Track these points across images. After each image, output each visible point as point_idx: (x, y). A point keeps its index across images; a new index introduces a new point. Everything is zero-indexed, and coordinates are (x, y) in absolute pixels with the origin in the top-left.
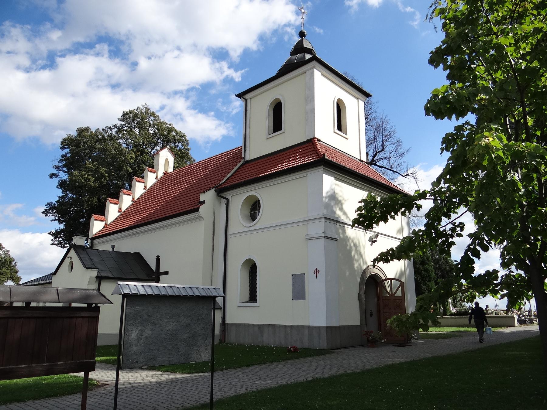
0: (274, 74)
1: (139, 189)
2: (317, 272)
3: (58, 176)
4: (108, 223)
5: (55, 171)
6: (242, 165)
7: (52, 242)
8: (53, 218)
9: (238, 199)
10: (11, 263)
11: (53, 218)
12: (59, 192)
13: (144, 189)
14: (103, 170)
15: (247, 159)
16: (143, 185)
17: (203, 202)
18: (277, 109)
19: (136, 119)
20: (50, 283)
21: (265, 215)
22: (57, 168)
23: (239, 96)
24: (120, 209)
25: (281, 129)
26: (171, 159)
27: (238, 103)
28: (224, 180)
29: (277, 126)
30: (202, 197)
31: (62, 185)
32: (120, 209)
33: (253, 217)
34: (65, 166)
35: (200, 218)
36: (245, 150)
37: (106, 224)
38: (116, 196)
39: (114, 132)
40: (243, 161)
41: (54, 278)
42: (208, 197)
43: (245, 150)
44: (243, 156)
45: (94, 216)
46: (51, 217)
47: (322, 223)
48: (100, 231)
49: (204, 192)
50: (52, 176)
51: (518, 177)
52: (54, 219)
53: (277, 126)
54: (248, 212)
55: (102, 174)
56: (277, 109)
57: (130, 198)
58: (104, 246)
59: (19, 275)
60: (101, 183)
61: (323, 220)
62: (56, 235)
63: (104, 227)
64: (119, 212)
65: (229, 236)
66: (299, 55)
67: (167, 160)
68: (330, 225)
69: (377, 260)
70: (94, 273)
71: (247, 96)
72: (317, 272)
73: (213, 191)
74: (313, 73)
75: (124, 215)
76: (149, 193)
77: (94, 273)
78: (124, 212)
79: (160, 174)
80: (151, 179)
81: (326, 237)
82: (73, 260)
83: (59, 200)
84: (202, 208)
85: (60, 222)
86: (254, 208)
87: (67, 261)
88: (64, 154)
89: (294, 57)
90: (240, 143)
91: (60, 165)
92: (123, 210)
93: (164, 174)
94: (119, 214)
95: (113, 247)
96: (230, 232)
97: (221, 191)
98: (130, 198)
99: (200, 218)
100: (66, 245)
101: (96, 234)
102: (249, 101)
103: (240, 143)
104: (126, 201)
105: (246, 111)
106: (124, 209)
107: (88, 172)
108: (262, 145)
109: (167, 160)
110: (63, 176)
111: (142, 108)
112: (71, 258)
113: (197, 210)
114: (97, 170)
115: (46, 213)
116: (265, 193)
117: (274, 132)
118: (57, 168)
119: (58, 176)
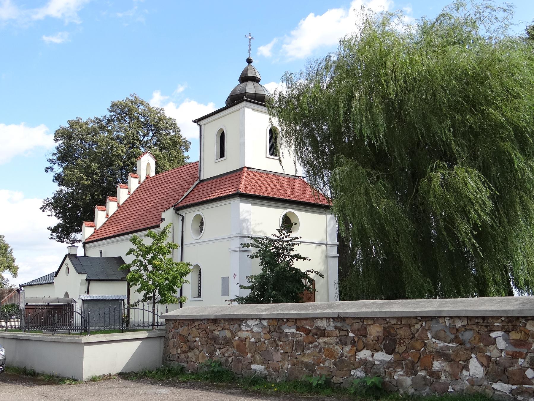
1: (123, 194)
3: (53, 169)
4: (97, 229)
5: (50, 165)
6: (197, 184)
7: (51, 237)
8: (50, 213)
9: (190, 215)
10: (6, 250)
11: (50, 213)
12: (56, 187)
13: (128, 194)
14: (94, 166)
15: (202, 178)
16: (127, 190)
19: (124, 111)
20: (53, 283)
22: (51, 161)
24: (107, 215)
26: (153, 162)
28: (182, 199)
30: (163, 215)
31: (58, 179)
32: (107, 215)
34: (58, 159)
37: (95, 229)
38: (103, 203)
39: (104, 123)
40: (198, 180)
41: (56, 280)
42: (168, 215)
45: (85, 224)
46: (48, 212)
48: (91, 236)
49: (164, 211)
50: (47, 170)
52: (50, 214)
55: (94, 170)
57: (116, 204)
58: (94, 252)
59: (16, 263)
60: (93, 179)
62: (55, 230)
63: (94, 232)
64: (106, 217)
67: (148, 164)
70: (84, 277)
71: (202, 123)
74: (244, 111)
75: (111, 220)
76: (132, 196)
77: (84, 277)
78: (111, 217)
79: (143, 178)
80: (134, 184)
82: (69, 266)
83: (54, 197)
85: (58, 217)
87: (64, 266)
88: (58, 145)
91: (55, 158)
92: (110, 216)
93: (147, 178)
94: (107, 219)
95: (101, 251)
97: (178, 209)
98: (116, 204)
100: (64, 240)
101: (87, 239)
102: (203, 127)
104: (112, 207)
105: (201, 136)
106: (110, 214)
107: (80, 170)
109: (148, 164)
110: (58, 169)
111: (130, 98)
112: (67, 264)
114: (88, 167)
115: (43, 209)
116: (207, 212)
118: (51, 161)
119: (53, 169)
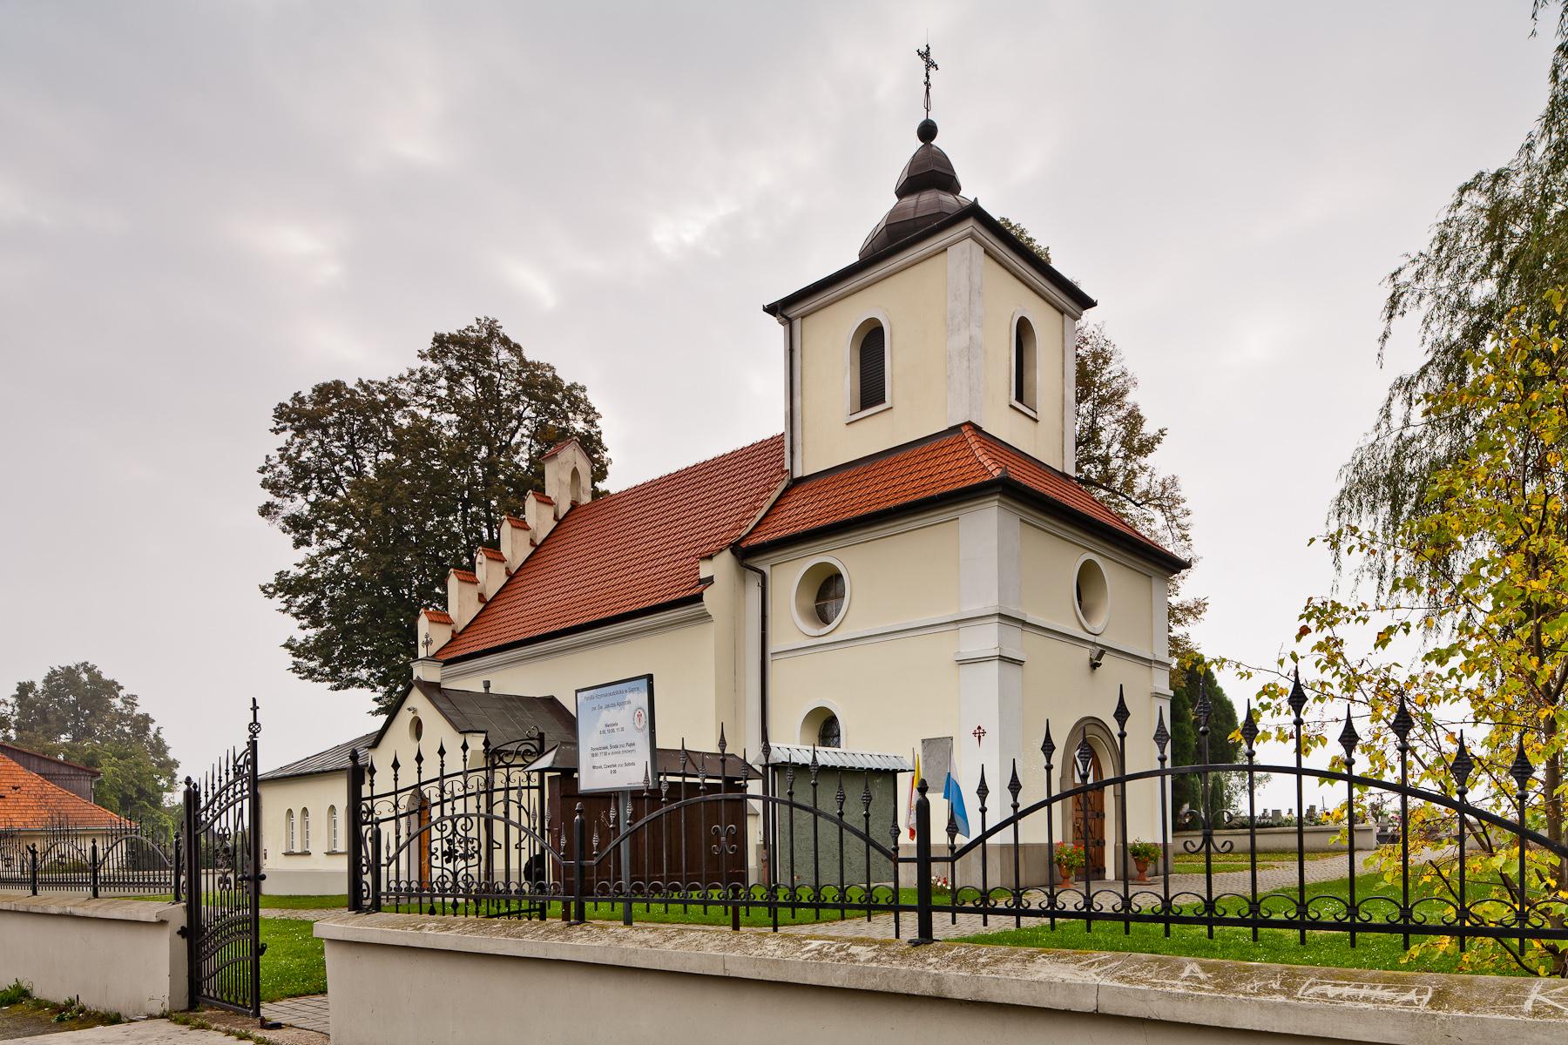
0: (854, 258)
2: (979, 733)
9: (788, 576)
15: (798, 474)
17: (710, 580)
18: (871, 341)
21: (855, 614)
23: (772, 309)
25: (883, 401)
27: (774, 329)
29: (871, 391)
33: (822, 617)
35: (705, 617)
36: (792, 452)
43: (792, 452)
44: (787, 466)
47: (993, 627)
51: (1397, 557)
53: (871, 391)
54: (810, 603)
56: (871, 341)
61: (997, 619)
65: (769, 658)
66: (927, 197)
68: (1015, 632)
69: (414, 711)
71: (794, 312)
72: (979, 733)
73: (727, 554)
81: (1002, 658)
84: (708, 594)
86: (825, 592)
89: (910, 201)
90: (778, 426)
96: (771, 649)
97: (747, 555)
99: (705, 617)
102: (797, 323)
103: (778, 426)
105: (791, 350)
108: (836, 438)
113: (698, 598)
117: (863, 407)
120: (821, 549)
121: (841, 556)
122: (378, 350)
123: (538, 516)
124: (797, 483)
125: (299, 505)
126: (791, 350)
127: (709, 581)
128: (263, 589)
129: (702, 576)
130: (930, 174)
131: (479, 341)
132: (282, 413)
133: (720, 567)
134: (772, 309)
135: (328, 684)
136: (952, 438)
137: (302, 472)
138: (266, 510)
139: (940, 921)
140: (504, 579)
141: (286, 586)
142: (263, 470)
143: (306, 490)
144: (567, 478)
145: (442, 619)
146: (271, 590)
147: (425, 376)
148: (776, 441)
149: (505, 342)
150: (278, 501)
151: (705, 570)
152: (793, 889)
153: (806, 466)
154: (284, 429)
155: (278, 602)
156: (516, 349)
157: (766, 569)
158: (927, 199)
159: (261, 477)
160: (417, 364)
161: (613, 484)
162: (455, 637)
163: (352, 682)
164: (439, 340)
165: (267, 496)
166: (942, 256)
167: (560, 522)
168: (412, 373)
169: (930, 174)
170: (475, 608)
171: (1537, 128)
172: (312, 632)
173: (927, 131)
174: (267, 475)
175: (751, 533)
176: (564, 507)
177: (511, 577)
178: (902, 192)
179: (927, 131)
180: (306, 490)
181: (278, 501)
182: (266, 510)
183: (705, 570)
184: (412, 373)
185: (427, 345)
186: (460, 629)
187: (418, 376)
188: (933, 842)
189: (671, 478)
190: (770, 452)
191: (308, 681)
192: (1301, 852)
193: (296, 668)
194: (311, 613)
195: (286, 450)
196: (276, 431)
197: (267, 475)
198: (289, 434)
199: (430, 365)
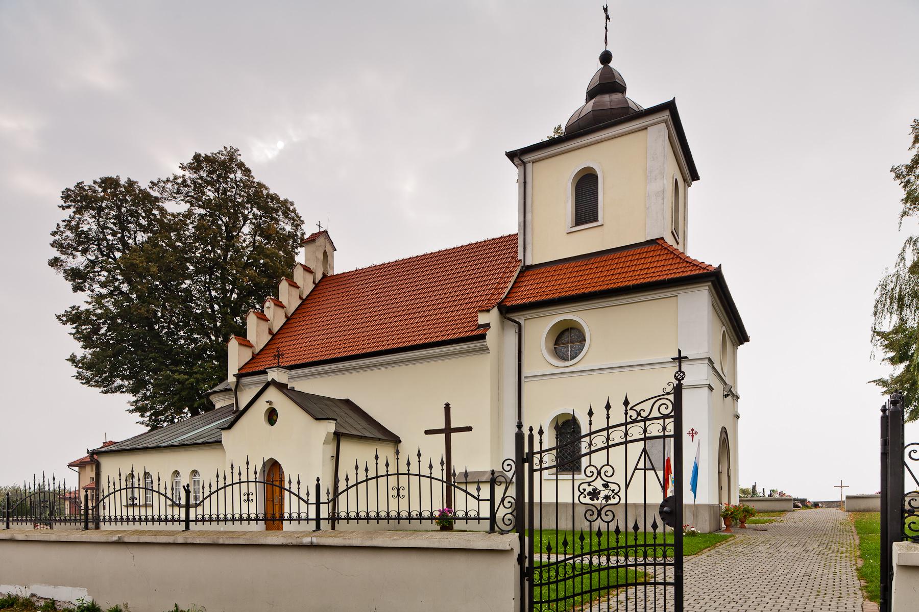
9: (539, 328)
15: (528, 263)
23: (511, 155)
25: (596, 220)
27: (512, 171)
35: (485, 349)
36: (525, 248)
43: (525, 248)
44: (520, 256)
54: (552, 346)
65: (523, 379)
71: (526, 158)
86: (567, 341)
97: (507, 311)
99: (485, 349)
102: (529, 166)
105: (525, 183)
108: (556, 239)
113: (483, 337)
117: (578, 223)
120: (572, 309)
121: (586, 317)
122: (157, 161)
123: (304, 279)
124: (527, 269)
125: (79, 261)
126: (525, 183)
127: (487, 326)
128: (59, 317)
129: (480, 322)
130: (608, 84)
131: (223, 162)
132: (66, 195)
133: (491, 318)
134: (511, 155)
135: (102, 389)
136: (653, 247)
137: (83, 241)
138: (55, 263)
139: (192, 524)
140: (284, 320)
141: (75, 317)
142: (54, 234)
143: (84, 252)
144: (321, 256)
145: (245, 343)
146: (64, 319)
147: (185, 181)
148: (513, 238)
149: (241, 165)
150: (63, 257)
151: (483, 319)
152: (290, 514)
153: (533, 259)
154: (69, 207)
155: (70, 328)
156: (247, 172)
157: (522, 321)
158: (608, 100)
159: (52, 239)
160: (180, 173)
161: (341, 265)
162: (254, 357)
163: (119, 389)
164: (197, 157)
165: (55, 253)
166: (645, 131)
167: (317, 285)
168: (176, 178)
169: (608, 84)
170: (267, 338)
171: (271, 192)
172: (88, 352)
173: (606, 58)
174: (57, 237)
175: (506, 297)
176: (319, 276)
177: (288, 319)
178: (591, 95)
179: (606, 58)
180: (84, 252)
181: (63, 257)
182: (55, 263)
183: (483, 319)
184: (176, 178)
185: (188, 159)
186: (258, 351)
187: (180, 181)
188: (685, 502)
189: (397, 264)
190: (506, 245)
191: (86, 386)
192: (256, 482)
193: (79, 376)
194: (87, 340)
195: (70, 222)
196: (63, 208)
197: (57, 237)
198: (70, 211)
199: (187, 174)
